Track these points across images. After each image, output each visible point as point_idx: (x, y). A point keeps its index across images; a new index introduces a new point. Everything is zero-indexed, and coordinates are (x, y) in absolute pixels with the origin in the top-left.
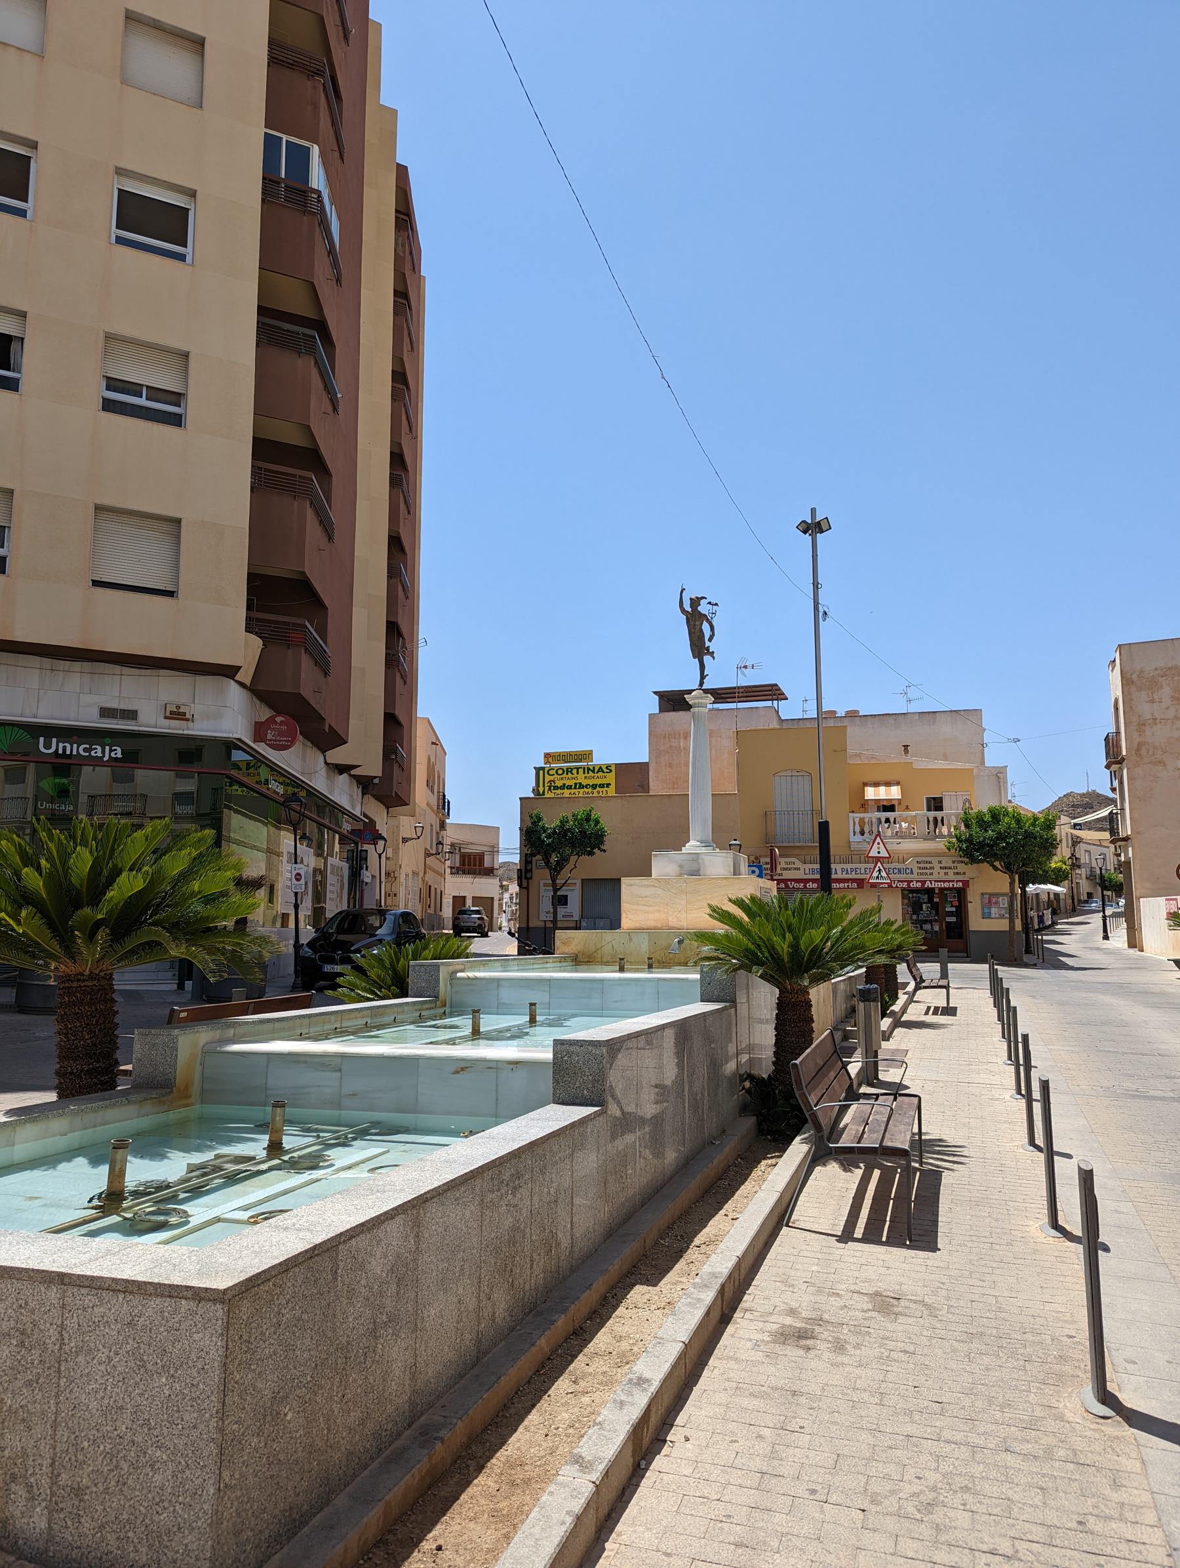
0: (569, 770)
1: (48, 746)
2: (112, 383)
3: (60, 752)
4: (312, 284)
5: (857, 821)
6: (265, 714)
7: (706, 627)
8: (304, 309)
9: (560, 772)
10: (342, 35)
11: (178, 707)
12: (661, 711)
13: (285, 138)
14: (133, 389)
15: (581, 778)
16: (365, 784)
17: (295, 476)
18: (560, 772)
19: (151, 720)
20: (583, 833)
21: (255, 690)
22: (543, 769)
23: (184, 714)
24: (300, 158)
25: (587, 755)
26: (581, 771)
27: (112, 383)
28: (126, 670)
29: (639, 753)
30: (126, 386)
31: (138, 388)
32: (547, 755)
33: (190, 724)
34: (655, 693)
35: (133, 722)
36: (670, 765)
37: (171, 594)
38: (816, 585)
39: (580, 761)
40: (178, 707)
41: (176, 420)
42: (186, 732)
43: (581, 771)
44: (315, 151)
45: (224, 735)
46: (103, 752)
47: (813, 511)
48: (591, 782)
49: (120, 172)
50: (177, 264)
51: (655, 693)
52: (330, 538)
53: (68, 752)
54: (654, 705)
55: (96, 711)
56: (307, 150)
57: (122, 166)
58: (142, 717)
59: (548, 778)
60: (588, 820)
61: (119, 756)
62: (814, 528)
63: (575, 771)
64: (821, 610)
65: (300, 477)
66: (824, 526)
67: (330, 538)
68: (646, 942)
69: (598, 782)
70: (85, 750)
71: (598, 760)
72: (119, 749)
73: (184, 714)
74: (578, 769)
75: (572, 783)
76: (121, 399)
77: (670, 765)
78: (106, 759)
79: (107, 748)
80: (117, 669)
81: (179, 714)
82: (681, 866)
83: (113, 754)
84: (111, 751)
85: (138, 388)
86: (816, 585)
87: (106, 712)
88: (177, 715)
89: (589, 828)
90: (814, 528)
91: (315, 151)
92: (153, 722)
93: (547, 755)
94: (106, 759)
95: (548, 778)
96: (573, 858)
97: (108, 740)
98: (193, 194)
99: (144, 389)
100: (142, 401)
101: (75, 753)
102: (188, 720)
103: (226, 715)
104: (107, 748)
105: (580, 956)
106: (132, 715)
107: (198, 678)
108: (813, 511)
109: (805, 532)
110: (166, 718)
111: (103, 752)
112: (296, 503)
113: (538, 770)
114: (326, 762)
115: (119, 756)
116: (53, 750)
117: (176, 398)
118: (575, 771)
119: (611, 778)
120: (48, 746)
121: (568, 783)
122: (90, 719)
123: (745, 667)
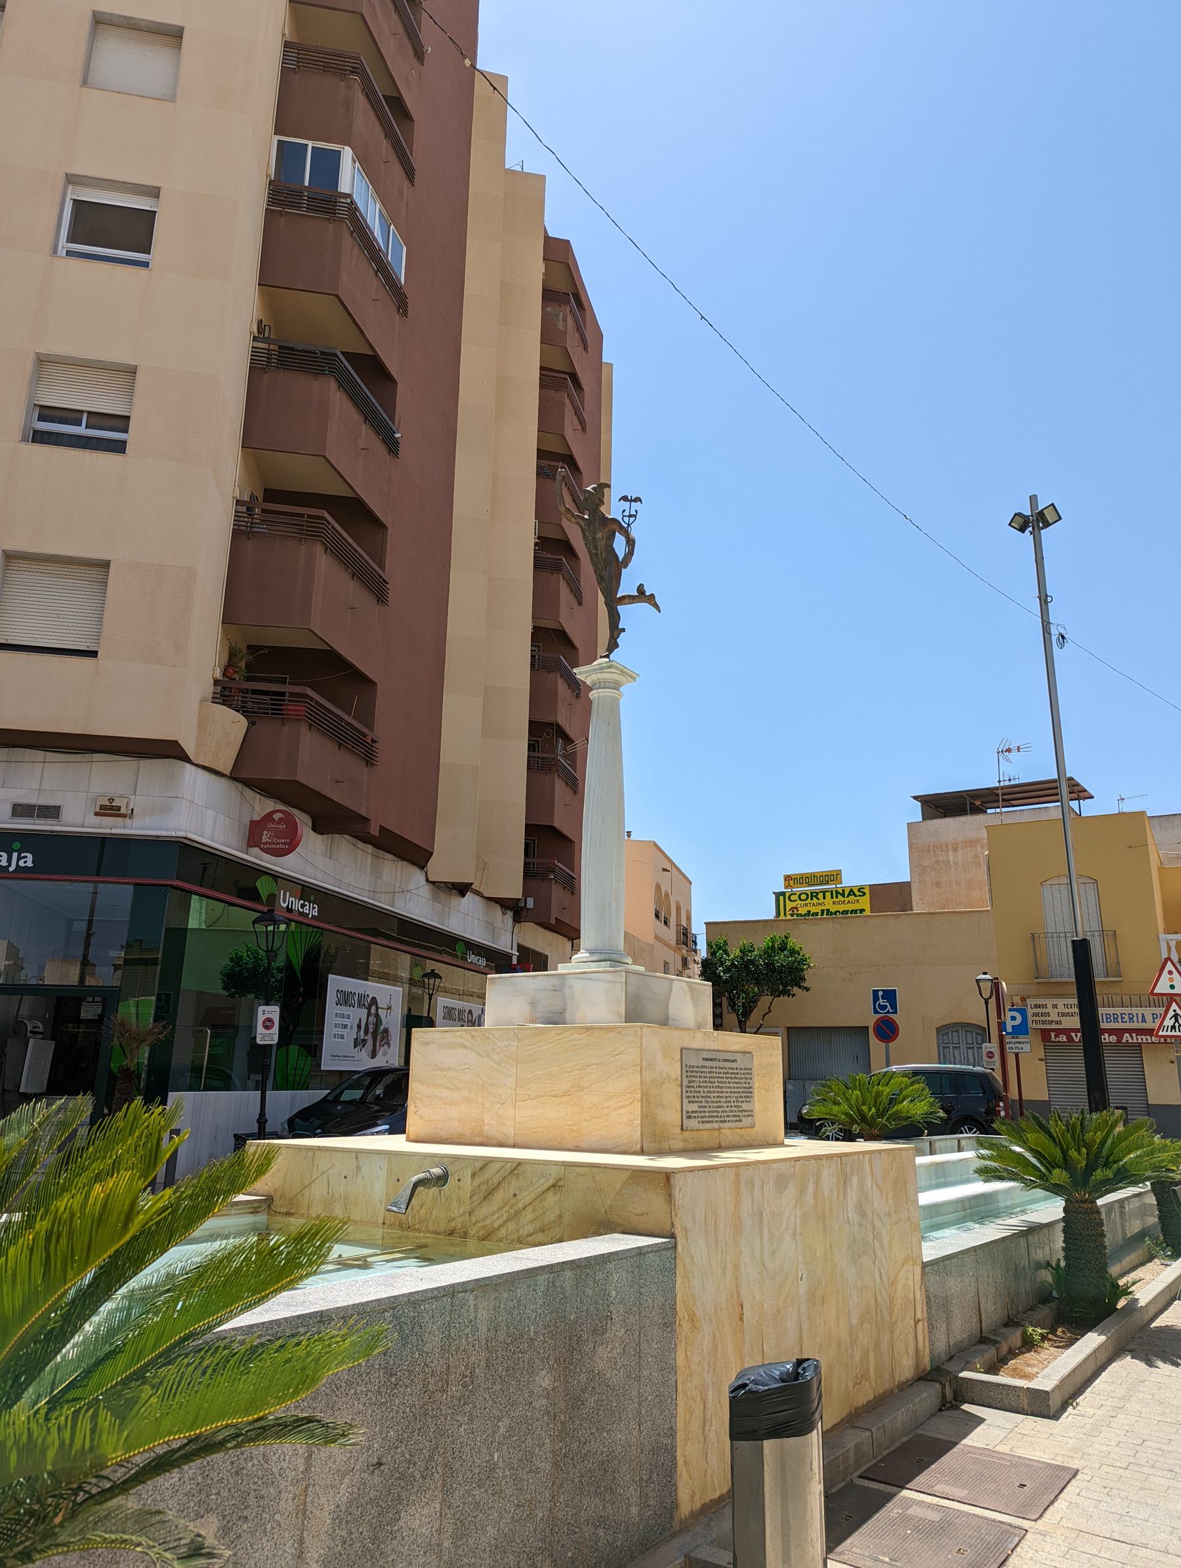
0: (814, 895)
2: (48, 412)
4: (337, 296)
5: (1173, 945)
6: (263, 806)
7: (619, 545)
8: (560, 450)
9: (804, 897)
10: (411, 52)
11: (112, 800)
12: (924, 819)
13: (310, 144)
14: (72, 416)
15: (829, 904)
16: (516, 910)
17: (302, 515)
18: (804, 897)
19: (78, 818)
20: (769, 965)
21: (243, 775)
22: (783, 894)
23: (119, 808)
24: (328, 164)
25: (835, 876)
26: (828, 895)
27: (48, 412)
28: (51, 756)
29: (900, 872)
30: (65, 414)
31: (74, 415)
32: (788, 878)
33: (128, 821)
34: (916, 798)
35: (54, 822)
36: (938, 885)
37: (93, 654)
38: (1044, 600)
39: (827, 883)
40: (112, 800)
41: (119, 447)
42: (114, 831)
43: (828, 895)
44: (347, 153)
45: (168, 834)
46: (9, 860)
47: (1033, 499)
48: (841, 908)
49: (72, 180)
50: (143, 272)
51: (916, 798)
54: (915, 812)
55: (8, 809)
56: (338, 154)
57: (75, 171)
58: (65, 815)
59: (789, 905)
60: (783, 948)
61: (30, 864)
62: (1034, 521)
63: (821, 896)
64: (1054, 632)
65: (309, 516)
66: (1050, 516)
68: (383, 1174)
69: (849, 907)
71: (848, 881)
72: (30, 856)
73: (119, 808)
74: (824, 893)
75: (818, 909)
76: (52, 427)
77: (938, 885)
78: (11, 869)
79: (15, 855)
80: (40, 755)
81: (112, 808)
82: (533, 1004)
83: (21, 863)
85: (74, 415)
86: (1044, 600)
87: (20, 810)
88: (109, 810)
89: (781, 959)
90: (1034, 521)
91: (347, 153)
93: (788, 878)
94: (11, 869)
95: (789, 905)
96: (765, 1000)
97: (17, 845)
98: (155, 192)
99: (85, 416)
100: (81, 430)
102: (124, 816)
103: (198, 810)
104: (15, 855)
105: (276, 1201)
106: (52, 812)
107: (145, 764)
108: (1033, 499)
109: (1022, 529)
110: (96, 814)
111: (9, 860)
112: (303, 547)
113: (778, 895)
114: (427, 880)
115: (30, 864)
117: (121, 422)
118: (821, 896)
119: (865, 903)
121: (813, 910)
123: (1009, 750)
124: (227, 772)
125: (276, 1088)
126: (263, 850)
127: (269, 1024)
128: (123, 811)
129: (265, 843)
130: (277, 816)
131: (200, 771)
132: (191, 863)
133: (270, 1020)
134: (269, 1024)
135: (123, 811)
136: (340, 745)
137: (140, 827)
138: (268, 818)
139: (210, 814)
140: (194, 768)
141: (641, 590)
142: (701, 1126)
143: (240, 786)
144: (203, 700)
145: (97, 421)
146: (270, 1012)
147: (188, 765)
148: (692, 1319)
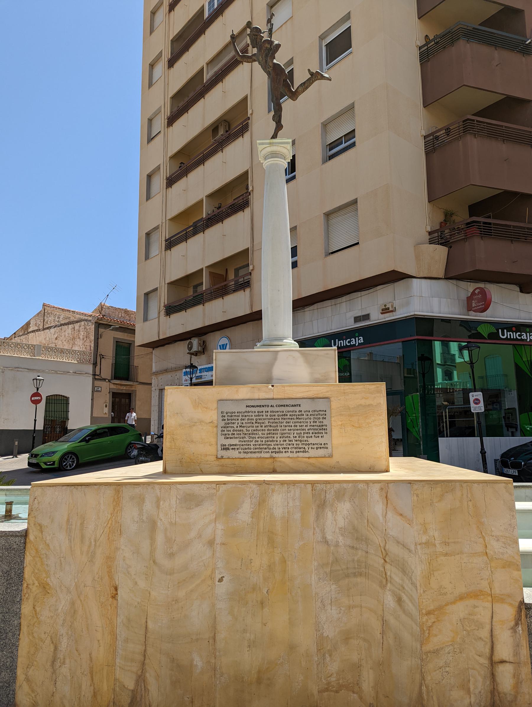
1: (503, 335)
3: (509, 337)
21: (453, 274)
28: (363, 293)
37: (358, 243)
42: (387, 319)
45: (406, 315)
46: (356, 342)
52: (151, 34)
53: (512, 337)
55: (353, 320)
58: (372, 317)
61: (362, 341)
67: (151, 34)
70: (519, 335)
78: (357, 345)
79: (357, 338)
80: (359, 294)
83: (360, 342)
84: (359, 340)
87: (357, 319)
88: (385, 311)
92: (377, 318)
94: (357, 345)
97: (528, 330)
101: (515, 338)
102: (392, 311)
103: (429, 299)
104: (357, 338)
106: (366, 317)
107: (396, 284)
110: (382, 313)
111: (356, 342)
115: (362, 341)
116: (505, 337)
120: (503, 335)
122: (351, 325)
124: (442, 275)
125: (488, 435)
126: (474, 311)
127: (477, 402)
128: (391, 309)
129: (474, 307)
130: (477, 292)
131: (423, 281)
132: (425, 327)
133: (477, 399)
134: (477, 402)
135: (391, 309)
136: (512, 241)
137: (400, 314)
138: (473, 293)
139: (435, 300)
140: (418, 280)
141: (312, 74)
142: (245, 455)
143: (454, 282)
144: (417, 245)
145: (347, 138)
146: (477, 395)
147: (414, 279)
148: (45, 588)
